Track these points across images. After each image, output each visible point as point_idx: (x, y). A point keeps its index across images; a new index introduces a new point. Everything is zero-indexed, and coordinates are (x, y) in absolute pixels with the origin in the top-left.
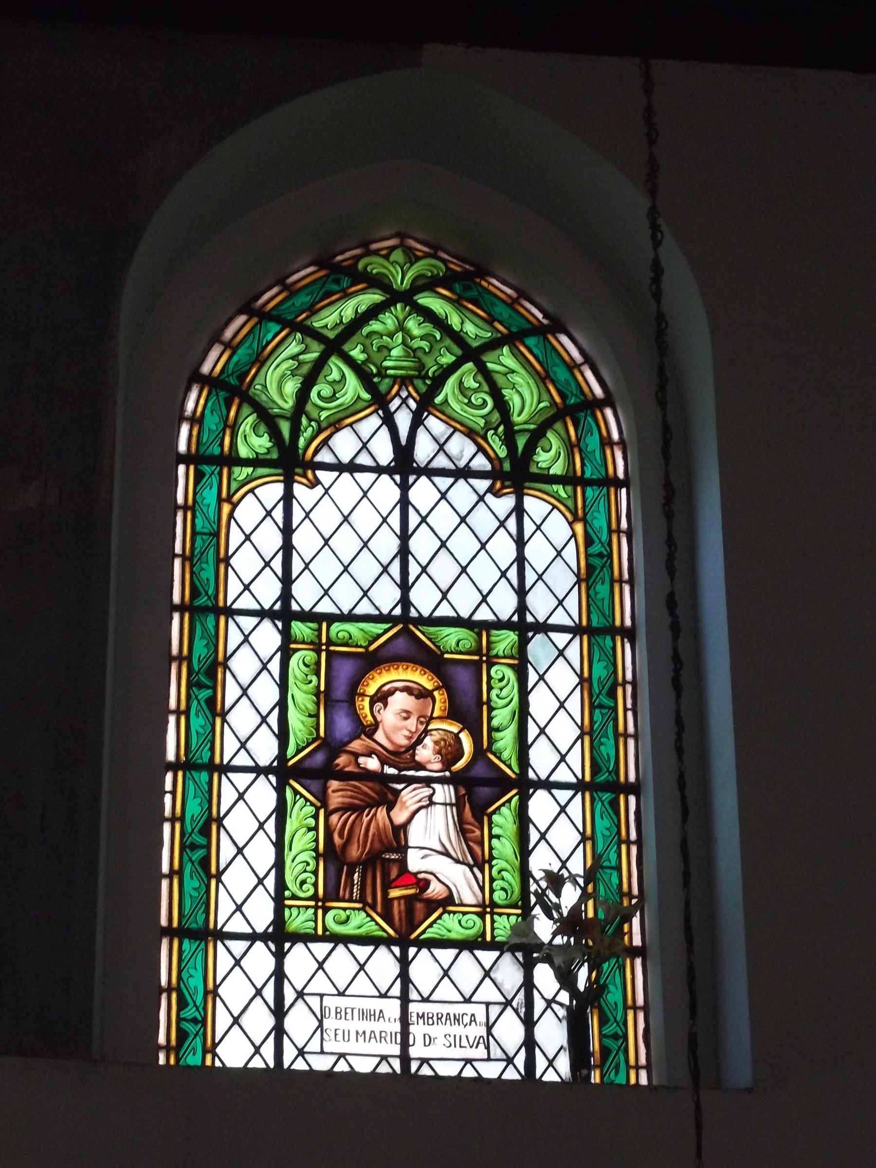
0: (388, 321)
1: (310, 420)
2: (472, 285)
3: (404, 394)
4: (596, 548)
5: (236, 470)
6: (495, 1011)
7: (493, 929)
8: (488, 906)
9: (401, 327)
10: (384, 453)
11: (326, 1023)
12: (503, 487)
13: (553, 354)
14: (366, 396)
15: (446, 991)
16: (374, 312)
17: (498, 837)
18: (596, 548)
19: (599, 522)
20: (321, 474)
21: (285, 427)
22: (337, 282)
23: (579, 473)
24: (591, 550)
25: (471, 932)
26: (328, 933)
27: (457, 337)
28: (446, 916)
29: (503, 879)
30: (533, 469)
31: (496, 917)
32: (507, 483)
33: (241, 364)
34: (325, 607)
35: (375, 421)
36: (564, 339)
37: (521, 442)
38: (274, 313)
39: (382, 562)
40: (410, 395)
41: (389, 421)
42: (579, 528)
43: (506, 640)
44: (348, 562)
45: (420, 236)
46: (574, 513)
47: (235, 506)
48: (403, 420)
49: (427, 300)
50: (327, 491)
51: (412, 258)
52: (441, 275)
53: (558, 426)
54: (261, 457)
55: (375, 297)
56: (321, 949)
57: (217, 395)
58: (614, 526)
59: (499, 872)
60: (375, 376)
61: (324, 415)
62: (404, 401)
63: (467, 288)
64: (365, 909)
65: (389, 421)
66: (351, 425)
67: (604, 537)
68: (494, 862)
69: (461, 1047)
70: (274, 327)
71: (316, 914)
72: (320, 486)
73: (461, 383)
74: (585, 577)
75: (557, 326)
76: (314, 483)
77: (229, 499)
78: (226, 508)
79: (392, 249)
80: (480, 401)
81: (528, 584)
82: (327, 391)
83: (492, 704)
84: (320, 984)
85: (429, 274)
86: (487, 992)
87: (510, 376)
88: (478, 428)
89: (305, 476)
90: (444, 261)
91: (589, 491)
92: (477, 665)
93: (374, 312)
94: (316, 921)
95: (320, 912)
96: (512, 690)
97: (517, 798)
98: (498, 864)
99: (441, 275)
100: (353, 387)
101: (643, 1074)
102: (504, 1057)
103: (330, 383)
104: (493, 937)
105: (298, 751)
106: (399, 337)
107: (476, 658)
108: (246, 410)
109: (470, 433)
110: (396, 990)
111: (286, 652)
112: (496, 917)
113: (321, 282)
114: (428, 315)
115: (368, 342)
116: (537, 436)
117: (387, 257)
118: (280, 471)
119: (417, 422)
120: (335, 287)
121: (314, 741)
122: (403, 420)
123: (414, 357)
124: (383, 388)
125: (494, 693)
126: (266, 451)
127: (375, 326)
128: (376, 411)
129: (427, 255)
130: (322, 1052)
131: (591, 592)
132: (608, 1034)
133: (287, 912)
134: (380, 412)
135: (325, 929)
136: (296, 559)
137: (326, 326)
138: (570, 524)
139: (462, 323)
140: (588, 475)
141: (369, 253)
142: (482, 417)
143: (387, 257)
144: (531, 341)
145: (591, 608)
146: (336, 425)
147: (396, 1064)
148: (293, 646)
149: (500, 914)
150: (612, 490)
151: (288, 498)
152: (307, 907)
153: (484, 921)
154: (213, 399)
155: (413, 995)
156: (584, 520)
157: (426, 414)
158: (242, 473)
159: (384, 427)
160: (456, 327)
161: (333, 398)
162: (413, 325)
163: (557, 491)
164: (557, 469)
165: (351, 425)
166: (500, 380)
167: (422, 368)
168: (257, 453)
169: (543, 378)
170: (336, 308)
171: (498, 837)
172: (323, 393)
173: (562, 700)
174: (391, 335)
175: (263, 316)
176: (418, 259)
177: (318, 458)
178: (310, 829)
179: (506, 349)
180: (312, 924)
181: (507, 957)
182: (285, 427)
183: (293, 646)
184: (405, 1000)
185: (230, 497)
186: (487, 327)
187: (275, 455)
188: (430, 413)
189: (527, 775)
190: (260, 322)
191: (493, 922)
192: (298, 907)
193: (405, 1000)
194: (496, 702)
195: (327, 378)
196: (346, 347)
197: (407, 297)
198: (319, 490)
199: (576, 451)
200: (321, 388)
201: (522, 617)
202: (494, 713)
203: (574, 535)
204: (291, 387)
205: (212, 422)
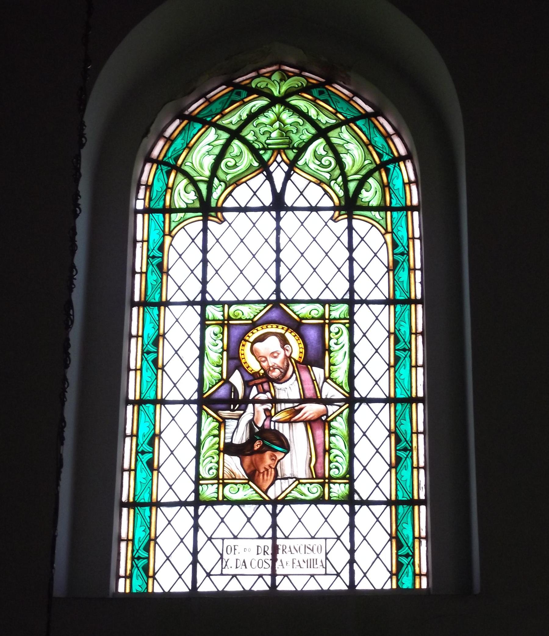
0: (271, 115)
1: (220, 181)
2: (325, 90)
3: (279, 159)
4: (400, 250)
5: (173, 215)
6: (330, 542)
7: (329, 492)
8: (327, 479)
9: (279, 119)
10: (268, 200)
11: (225, 556)
12: (340, 215)
13: (375, 130)
14: (256, 164)
15: (300, 532)
16: (262, 110)
17: (334, 435)
18: (400, 250)
19: (402, 233)
20: (226, 215)
21: (203, 187)
22: (239, 94)
23: (388, 204)
24: (396, 251)
25: (316, 495)
26: (225, 499)
27: (314, 123)
28: (300, 485)
29: (337, 462)
30: (359, 203)
31: (331, 485)
32: (343, 212)
33: (177, 150)
34: (228, 297)
35: (261, 177)
36: (382, 120)
37: (352, 186)
38: (200, 116)
39: (265, 268)
40: (283, 160)
41: (270, 178)
42: (388, 237)
43: (341, 310)
44: (248, 184)
45: (293, 61)
46: (386, 230)
47: (173, 237)
48: (279, 176)
49: (295, 101)
50: (230, 225)
51: (285, 76)
52: (304, 85)
53: (376, 174)
54: (190, 206)
55: (262, 102)
56: (222, 509)
57: (162, 170)
58: (410, 236)
59: (335, 457)
60: (261, 149)
61: (229, 177)
62: (279, 164)
63: (321, 93)
64: (251, 321)
65: (270, 178)
66: (245, 182)
67: (405, 243)
68: (332, 451)
69: (313, 568)
70: (198, 126)
71: (218, 488)
72: (226, 222)
73: (315, 151)
74: (392, 268)
75: (377, 113)
76: (222, 221)
77: (170, 234)
78: (168, 239)
79: (273, 72)
80: (327, 163)
81: (356, 275)
82: (232, 163)
83: (331, 349)
84: (223, 532)
85: (297, 86)
86: (326, 532)
87: (346, 145)
88: (325, 180)
89: (217, 217)
90: (306, 77)
91: (395, 214)
92: (322, 326)
93: (262, 110)
94: (218, 493)
95: (221, 486)
96: (345, 339)
97: (347, 410)
98: (334, 452)
99: (304, 85)
100: (248, 159)
101: (424, 580)
102: (336, 573)
103: (233, 158)
104: (329, 497)
105: (210, 388)
106: (277, 125)
107: (322, 321)
108: (180, 177)
109: (320, 183)
110: (270, 534)
111: (204, 324)
112: (331, 485)
113: (229, 94)
114: (296, 110)
115: (257, 130)
116: (362, 183)
117: (269, 78)
118: (200, 214)
119: (288, 177)
120: (238, 98)
121: (220, 381)
122: (279, 176)
123: (286, 136)
124: (266, 157)
125: (332, 343)
126: (192, 202)
127: (262, 119)
128: (262, 172)
129: (295, 75)
130: (222, 574)
131: (396, 277)
132: (403, 554)
133: (200, 487)
134: (265, 173)
135: (224, 497)
136: (209, 268)
137: (231, 123)
138: (383, 235)
139: (318, 115)
140: (393, 205)
141: (259, 76)
142: (328, 172)
143: (269, 78)
144: (360, 123)
145: (396, 287)
146: (236, 182)
147: (268, 579)
148: (207, 322)
149: (334, 483)
150: (409, 213)
151: (205, 230)
152: (212, 484)
153: (324, 488)
154: (159, 171)
155: (279, 534)
156: (392, 232)
157: (292, 172)
158: (176, 217)
159: (267, 181)
160: (314, 117)
161: (235, 166)
162: (288, 117)
163: (375, 216)
164: (375, 203)
165: (245, 182)
166: (340, 149)
167: (291, 141)
168: (187, 204)
169: (367, 145)
170: (157, 224)
171: (334, 435)
172: (229, 164)
173: (301, 191)
174: (272, 125)
175: (192, 119)
176: (289, 77)
177: (226, 205)
178: (215, 436)
179: (344, 128)
180: (216, 495)
181: (289, 205)
182: (203, 187)
183: (207, 322)
184: (274, 538)
185: (170, 232)
186: (333, 117)
187: (197, 205)
188: (295, 172)
189: (354, 395)
190: (189, 123)
191: (330, 488)
192: (207, 484)
193: (274, 538)
194: (334, 347)
195: (231, 154)
196: (243, 133)
197: (282, 101)
198: (225, 224)
199: (387, 190)
200: (228, 160)
201: (352, 296)
202: (331, 355)
203: (386, 242)
204: (209, 161)
205: (158, 186)
